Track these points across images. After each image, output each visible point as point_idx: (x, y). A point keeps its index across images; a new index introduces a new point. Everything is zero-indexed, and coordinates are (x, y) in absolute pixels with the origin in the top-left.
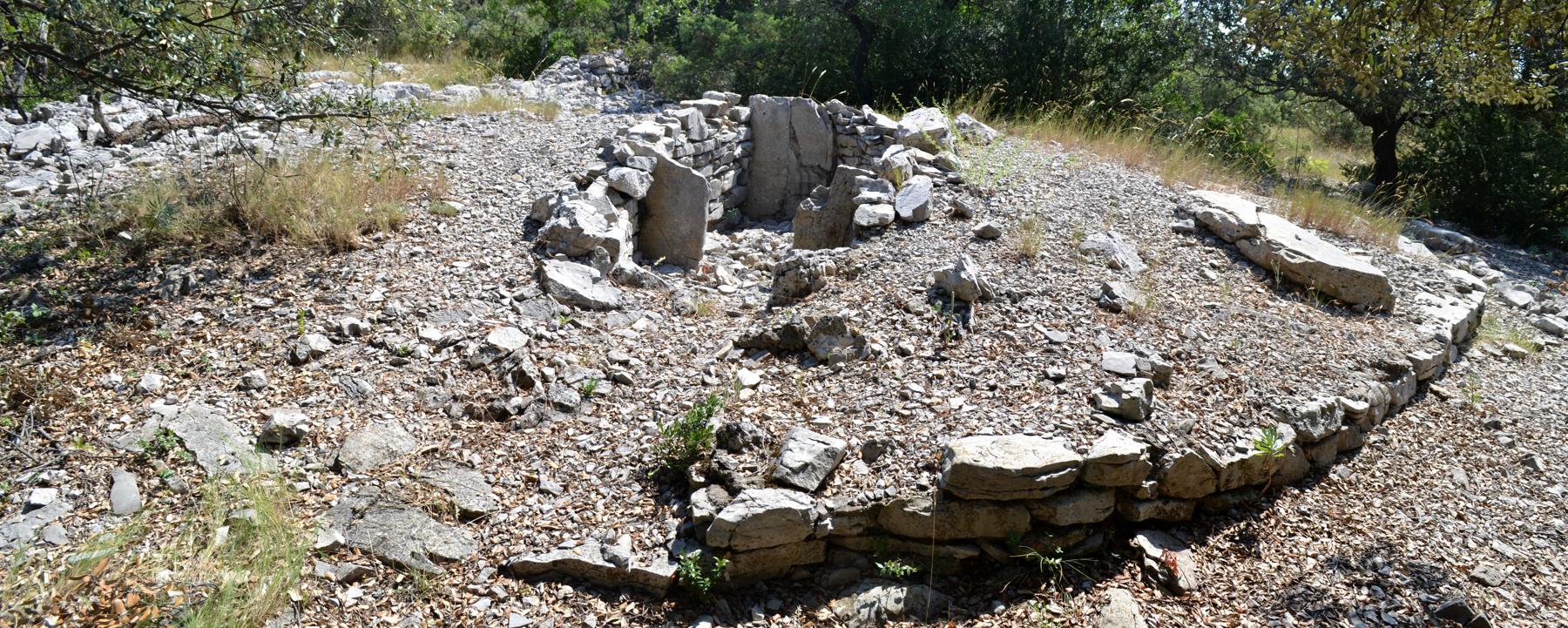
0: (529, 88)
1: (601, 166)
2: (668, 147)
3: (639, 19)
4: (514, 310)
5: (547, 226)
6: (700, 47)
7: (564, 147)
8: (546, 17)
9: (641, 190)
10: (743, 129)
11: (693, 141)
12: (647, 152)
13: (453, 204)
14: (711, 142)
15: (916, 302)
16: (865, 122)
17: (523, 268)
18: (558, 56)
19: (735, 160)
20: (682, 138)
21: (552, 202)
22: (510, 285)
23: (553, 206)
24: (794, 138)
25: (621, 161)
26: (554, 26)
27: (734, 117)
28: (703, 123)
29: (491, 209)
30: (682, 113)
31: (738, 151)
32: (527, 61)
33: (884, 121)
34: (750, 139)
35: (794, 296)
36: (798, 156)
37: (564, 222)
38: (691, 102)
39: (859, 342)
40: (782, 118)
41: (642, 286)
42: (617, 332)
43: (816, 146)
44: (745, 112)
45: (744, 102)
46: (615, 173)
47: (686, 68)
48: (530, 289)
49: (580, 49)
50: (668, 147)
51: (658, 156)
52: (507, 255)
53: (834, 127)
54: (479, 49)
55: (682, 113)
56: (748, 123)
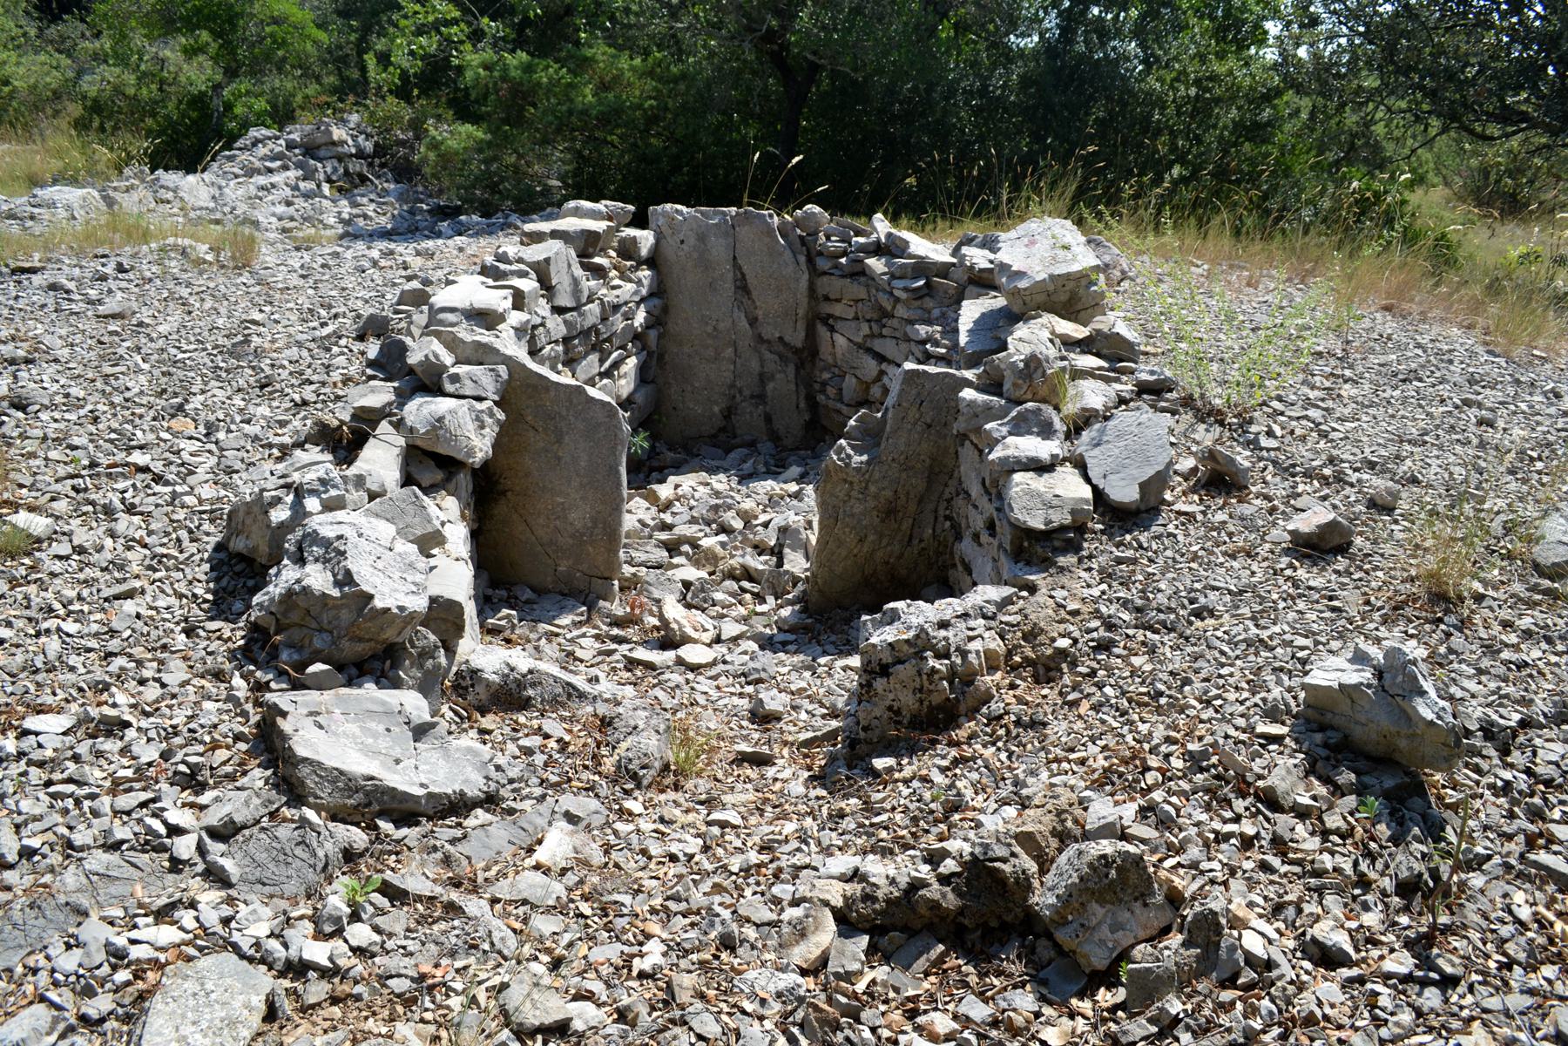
0: (194, 187)
1: (379, 394)
2: (520, 331)
3: (384, 59)
4: (215, 876)
5: (275, 590)
6: (504, 110)
7: (282, 337)
8: (215, 59)
9: (480, 445)
10: (645, 274)
11: (558, 310)
12: (482, 355)
13: (22, 518)
14: (594, 308)
15: (1283, 772)
16: (878, 250)
17: (217, 716)
18: (245, 126)
19: (637, 337)
20: (543, 307)
21: (279, 515)
22: (192, 781)
23: (286, 528)
24: (742, 287)
25: (428, 382)
26: (232, 73)
27: (627, 250)
28: (579, 272)
29: (124, 523)
30: (536, 253)
31: (640, 318)
32: (191, 139)
33: (927, 247)
34: (658, 293)
36: (753, 322)
37: (318, 578)
38: (545, 227)
39: (1207, 933)
40: (718, 249)
41: (524, 705)
42: (503, 889)
43: (781, 295)
44: (645, 239)
45: (640, 221)
46: (420, 410)
47: (480, 147)
48: (246, 797)
49: (281, 116)
50: (520, 331)
51: (508, 361)
52: (176, 673)
53: (810, 261)
54: (99, 117)
55: (536, 253)
56: (652, 262)
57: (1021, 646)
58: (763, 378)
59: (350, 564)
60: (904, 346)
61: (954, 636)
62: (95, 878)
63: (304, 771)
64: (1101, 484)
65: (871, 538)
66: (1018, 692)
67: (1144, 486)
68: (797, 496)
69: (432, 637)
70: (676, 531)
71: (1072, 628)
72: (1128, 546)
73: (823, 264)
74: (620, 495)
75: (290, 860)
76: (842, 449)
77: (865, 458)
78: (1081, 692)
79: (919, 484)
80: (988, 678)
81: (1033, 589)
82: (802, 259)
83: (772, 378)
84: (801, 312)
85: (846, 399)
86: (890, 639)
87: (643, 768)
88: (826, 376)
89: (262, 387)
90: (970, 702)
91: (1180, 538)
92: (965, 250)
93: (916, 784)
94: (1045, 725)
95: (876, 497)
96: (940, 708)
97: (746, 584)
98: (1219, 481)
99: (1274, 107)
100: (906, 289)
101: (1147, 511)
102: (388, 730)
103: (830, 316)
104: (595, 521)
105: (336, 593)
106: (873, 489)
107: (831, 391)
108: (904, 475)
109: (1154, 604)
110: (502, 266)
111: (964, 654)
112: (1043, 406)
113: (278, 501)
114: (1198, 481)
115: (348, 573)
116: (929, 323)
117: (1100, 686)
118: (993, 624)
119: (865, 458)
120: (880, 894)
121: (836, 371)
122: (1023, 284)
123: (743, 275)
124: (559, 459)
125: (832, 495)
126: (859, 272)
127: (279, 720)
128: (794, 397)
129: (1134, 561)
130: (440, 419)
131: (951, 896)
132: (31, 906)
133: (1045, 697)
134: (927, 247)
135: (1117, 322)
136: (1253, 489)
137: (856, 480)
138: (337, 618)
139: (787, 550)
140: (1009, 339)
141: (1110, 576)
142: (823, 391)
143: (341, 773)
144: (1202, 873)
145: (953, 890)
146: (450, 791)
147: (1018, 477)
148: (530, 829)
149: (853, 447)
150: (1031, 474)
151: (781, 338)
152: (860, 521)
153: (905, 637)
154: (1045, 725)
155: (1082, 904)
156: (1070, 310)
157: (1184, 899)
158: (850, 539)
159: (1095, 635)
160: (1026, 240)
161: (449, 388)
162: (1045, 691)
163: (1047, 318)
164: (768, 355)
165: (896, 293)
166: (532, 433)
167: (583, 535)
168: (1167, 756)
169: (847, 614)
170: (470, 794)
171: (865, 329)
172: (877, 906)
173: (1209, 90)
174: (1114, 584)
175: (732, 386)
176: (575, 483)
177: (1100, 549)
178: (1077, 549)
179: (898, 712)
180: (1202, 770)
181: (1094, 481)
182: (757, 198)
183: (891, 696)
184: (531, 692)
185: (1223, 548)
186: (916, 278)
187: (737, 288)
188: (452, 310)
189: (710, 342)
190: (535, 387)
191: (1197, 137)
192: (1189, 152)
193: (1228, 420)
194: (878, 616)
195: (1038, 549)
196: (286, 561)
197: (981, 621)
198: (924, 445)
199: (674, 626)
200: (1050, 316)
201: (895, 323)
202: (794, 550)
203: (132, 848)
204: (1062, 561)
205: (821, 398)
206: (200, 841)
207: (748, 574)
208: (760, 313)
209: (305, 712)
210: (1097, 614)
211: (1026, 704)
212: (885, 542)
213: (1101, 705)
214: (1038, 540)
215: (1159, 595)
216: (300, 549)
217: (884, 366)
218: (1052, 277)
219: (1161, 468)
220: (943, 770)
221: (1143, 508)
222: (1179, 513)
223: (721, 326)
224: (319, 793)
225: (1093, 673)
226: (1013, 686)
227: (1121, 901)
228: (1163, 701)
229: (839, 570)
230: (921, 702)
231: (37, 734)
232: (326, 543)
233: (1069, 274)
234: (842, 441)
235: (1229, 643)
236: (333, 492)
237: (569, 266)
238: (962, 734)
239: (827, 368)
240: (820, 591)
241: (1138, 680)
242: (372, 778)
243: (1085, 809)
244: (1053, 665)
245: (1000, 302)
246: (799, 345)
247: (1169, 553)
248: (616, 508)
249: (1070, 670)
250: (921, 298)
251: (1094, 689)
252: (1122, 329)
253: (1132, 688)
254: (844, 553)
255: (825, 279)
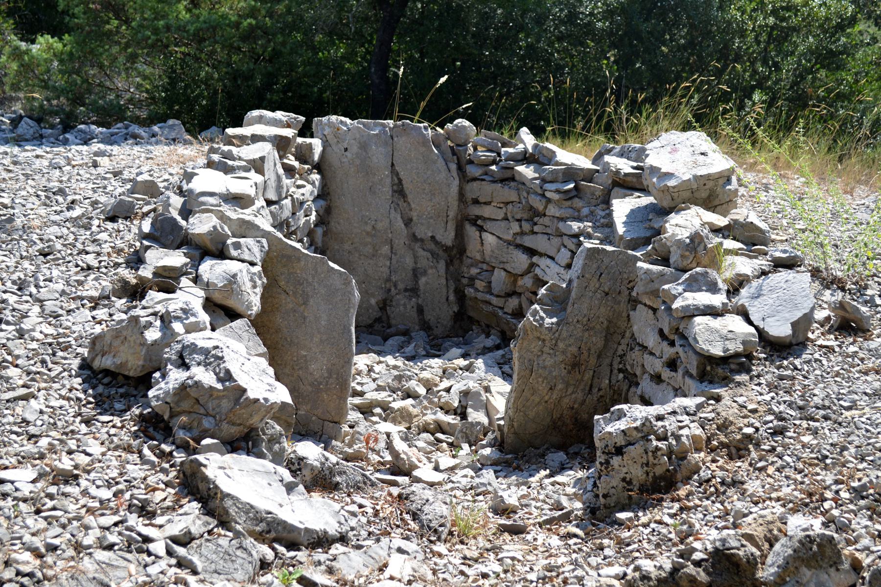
10: (316, 177)
12: (246, 229)
16: (526, 158)
21: (153, 335)
24: (399, 191)
33: (571, 156)
34: (323, 194)
35: (643, 489)
36: (408, 222)
37: (206, 377)
40: (379, 156)
51: (266, 234)
53: (460, 168)
56: (318, 167)
57: (717, 434)
58: (416, 274)
59: (229, 365)
60: (556, 241)
61: (670, 424)
62: (104, 566)
63: (228, 503)
64: (761, 325)
65: (560, 386)
66: (719, 464)
67: (794, 325)
68: (469, 368)
69: (278, 428)
70: (367, 396)
71: (754, 421)
72: (786, 368)
73: (473, 171)
74: (351, 350)
75: (234, 558)
76: (535, 312)
77: (555, 320)
78: (767, 461)
79: (597, 341)
80: (696, 455)
81: (718, 399)
82: (453, 167)
83: (425, 273)
84: (452, 214)
85: (495, 291)
86: (623, 427)
87: (440, 526)
88: (474, 271)
89: (45, 255)
90: (684, 472)
91: (825, 362)
92: (607, 158)
93: (653, 525)
94: (743, 483)
95: (563, 352)
96: (662, 477)
97: (440, 436)
98: (848, 325)
99: (848, 36)
100: (558, 191)
101: (797, 345)
102: (270, 484)
103: (478, 217)
104: (330, 372)
105: (219, 386)
106: (561, 345)
107: (480, 285)
108: (586, 334)
109: (812, 404)
110: (230, 163)
111: (678, 438)
112: (709, 270)
113: (149, 325)
114: (832, 326)
115: (228, 372)
116: (579, 219)
117: (780, 457)
118: (695, 418)
119: (555, 320)
120: (653, 576)
121: (485, 267)
122: (672, 183)
123: (400, 180)
124: (305, 318)
125: (528, 350)
126: (509, 178)
127: (202, 468)
128: (444, 290)
129: (793, 378)
130: (234, 276)
131: (703, 574)
132: (72, 577)
133: (739, 467)
134: (571, 156)
135: (744, 213)
136: (875, 332)
137: (547, 338)
138: (219, 406)
139: (469, 410)
140: (667, 225)
141: (776, 387)
142: (471, 285)
143: (252, 507)
144: (873, 552)
145: (704, 570)
146: (318, 529)
147: (698, 319)
148: (377, 558)
149: (545, 311)
150: (708, 317)
151: (433, 237)
152: (551, 372)
153: (634, 425)
154: (743, 483)
155: (796, 568)
156: (711, 203)
157: (863, 567)
158: (543, 388)
159: (771, 425)
160: (669, 149)
161: (234, 253)
162: (739, 464)
163: (695, 210)
164: (421, 253)
165: (548, 194)
166: (283, 296)
167: (321, 383)
168: (837, 492)
169: (541, 451)
170: (330, 533)
171: (515, 227)
172: (651, 583)
173: (783, 19)
174: (781, 392)
175: (388, 280)
176: (316, 339)
177: (769, 372)
178: (748, 371)
179: (630, 483)
180: (863, 498)
181: (756, 323)
182: (408, 110)
183: (625, 470)
184: (338, 479)
185: (858, 368)
186: (566, 182)
187: (394, 191)
188: (212, 194)
189: (369, 240)
190: (289, 258)
191: (776, 64)
192: (768, 78)
193: (848, 287)
194: (608, 415)
195: (717, 371)
196: (169, 367)
197: (685, 417)
198: (603, 310)
199: (403, 456)
200: (697, 208)
201: (546, 221)
202: (476, 410)
203: (120, 550)
204: (738, 378)
205: (469, 291)
206: (167, 546)
207: (440, 427)
208: (414, 215)
209: (217, 466)
210: (770, 411)
211: (727, 471)
212: (570, 390)
213: (783, 467)
214: (718, 365)
215: (815, 398)
216: (181, 357)
217: (535, 259)
218: (696, 177)
219: (807, 311)
220: (673, 516)
221: (794, 342)
222: (821, 346)
223: (380, 226)
224: (238, 520)
225: (773, 449)
226: (714, 461)
227: (821, 567)
228: (828, 461)
229: (532, 414)
230: (647, 473)
231: (12, 482)
232: (206, 352)
233: (709, 175)
234: (536, 306)
235: (871, 425)
236: (192, 319)
237: (275, 165)
238: (682, 492)
239: (475, 264)
240: (515, 433)
241: (807, 450)
242: (270, 513)
243: (785, 523)
244: (742, 446)
245: (646, 200)
246: (449, 243)
247: (818, 372)
248: (349, 362)
249: (756, 449)
250: (570, 198)
251: (776, 459)
252: (753, 218)
253: (804, 456)
254: (537, 400)
255: (475, 184)
